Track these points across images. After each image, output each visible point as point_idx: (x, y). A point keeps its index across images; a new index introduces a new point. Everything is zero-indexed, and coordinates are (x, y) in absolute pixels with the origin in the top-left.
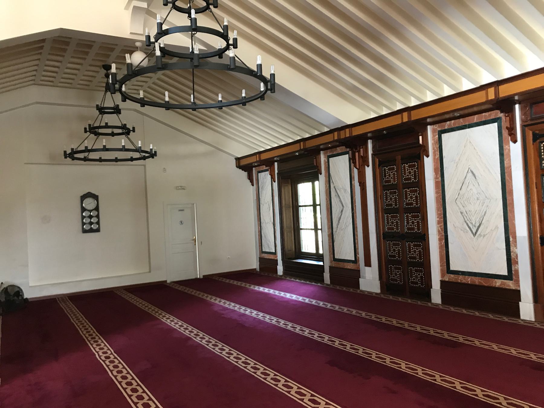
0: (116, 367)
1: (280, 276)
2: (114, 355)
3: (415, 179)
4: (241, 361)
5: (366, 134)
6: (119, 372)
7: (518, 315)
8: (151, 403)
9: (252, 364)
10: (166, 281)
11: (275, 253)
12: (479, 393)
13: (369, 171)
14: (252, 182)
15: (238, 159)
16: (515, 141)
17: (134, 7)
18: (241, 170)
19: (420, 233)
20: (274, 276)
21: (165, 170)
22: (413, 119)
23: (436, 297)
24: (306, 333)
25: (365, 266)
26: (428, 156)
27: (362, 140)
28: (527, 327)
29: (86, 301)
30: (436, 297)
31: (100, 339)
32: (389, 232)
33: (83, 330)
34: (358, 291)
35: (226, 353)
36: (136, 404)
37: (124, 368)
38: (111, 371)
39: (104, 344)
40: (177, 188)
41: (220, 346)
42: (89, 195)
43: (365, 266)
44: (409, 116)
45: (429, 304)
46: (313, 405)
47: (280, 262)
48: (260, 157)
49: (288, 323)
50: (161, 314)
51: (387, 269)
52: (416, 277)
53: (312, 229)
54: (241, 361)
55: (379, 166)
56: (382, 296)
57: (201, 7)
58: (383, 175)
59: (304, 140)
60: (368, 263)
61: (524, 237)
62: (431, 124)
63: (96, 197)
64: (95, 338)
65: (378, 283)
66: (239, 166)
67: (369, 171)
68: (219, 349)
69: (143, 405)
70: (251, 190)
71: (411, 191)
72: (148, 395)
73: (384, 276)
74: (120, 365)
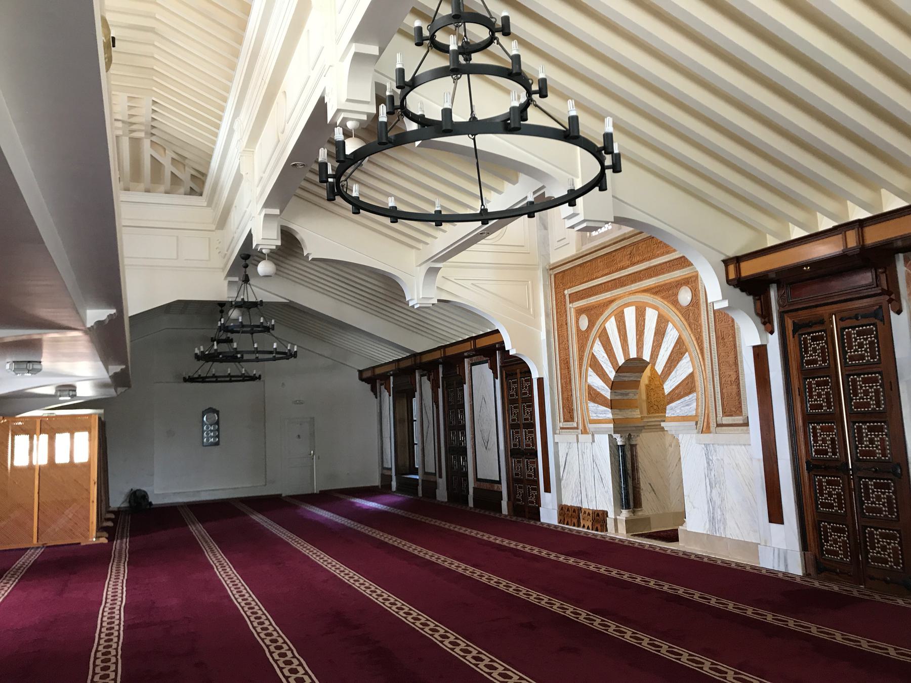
0: (279, 648)
1: (506, 516)
2: (292, 652)
3: (873, 357)
4: (460, 647)
5: (494, 345)
6: (271, 635)
7: (435, 497)
8: (306, 678)
9: (501, 669)
10: (281, 495)
11: (499, 482)
12: (707, 666)
13: (440, 390)
14: (376, 394)
15: (361, 372)
16: (772, 332)
17: (266, 215)
18: (738, 290)
19: (837, 460)
20: (497, 515)
21: (283, 384)
22: (478, 346)
23: (471, 504)
24: (598, 621)
25: (770, 522)
26: (899, 312)
27: (384, 378)
28: (440, 505)
29: (206, 511)
30: (471, 504)
31: (301, 664)
32: (819, 459)
33: (246, 609)
34: (538, 523)
35: (461, 650)
36: (287, 678)
37: (285, 642)
38: (281, 669)
39: (200, 527)
40: (295, 402)
41: (452, 638)
42: (212, 410)
43: (770, 522)
44: (861, 237)
45: (497, 515)
46: (501, 679)
47: (394, 478)
48: (445, 352)
49: (566, 605)
50: (394, 604)
51: (817, 527)
52: (835, 542)
53: (72, 438)
54: (460, 647)
55: (794, 332)
56: (514, 519)
57: (478, 41)
58: (804, 348)
59: (398, 360)
60: (441, 477)
61: (759, 460)
62: (467, 357)
63: (217, 412)
64: (263, 623)
65: (446, 494)
66: (361, 379)
67: (440, 390)
68: (450, 643)
69: (296, 679)
70: (376, 402)
71: (865, 381)
72: (303, 669)
73: (812, 543)
74: (285, 646)
